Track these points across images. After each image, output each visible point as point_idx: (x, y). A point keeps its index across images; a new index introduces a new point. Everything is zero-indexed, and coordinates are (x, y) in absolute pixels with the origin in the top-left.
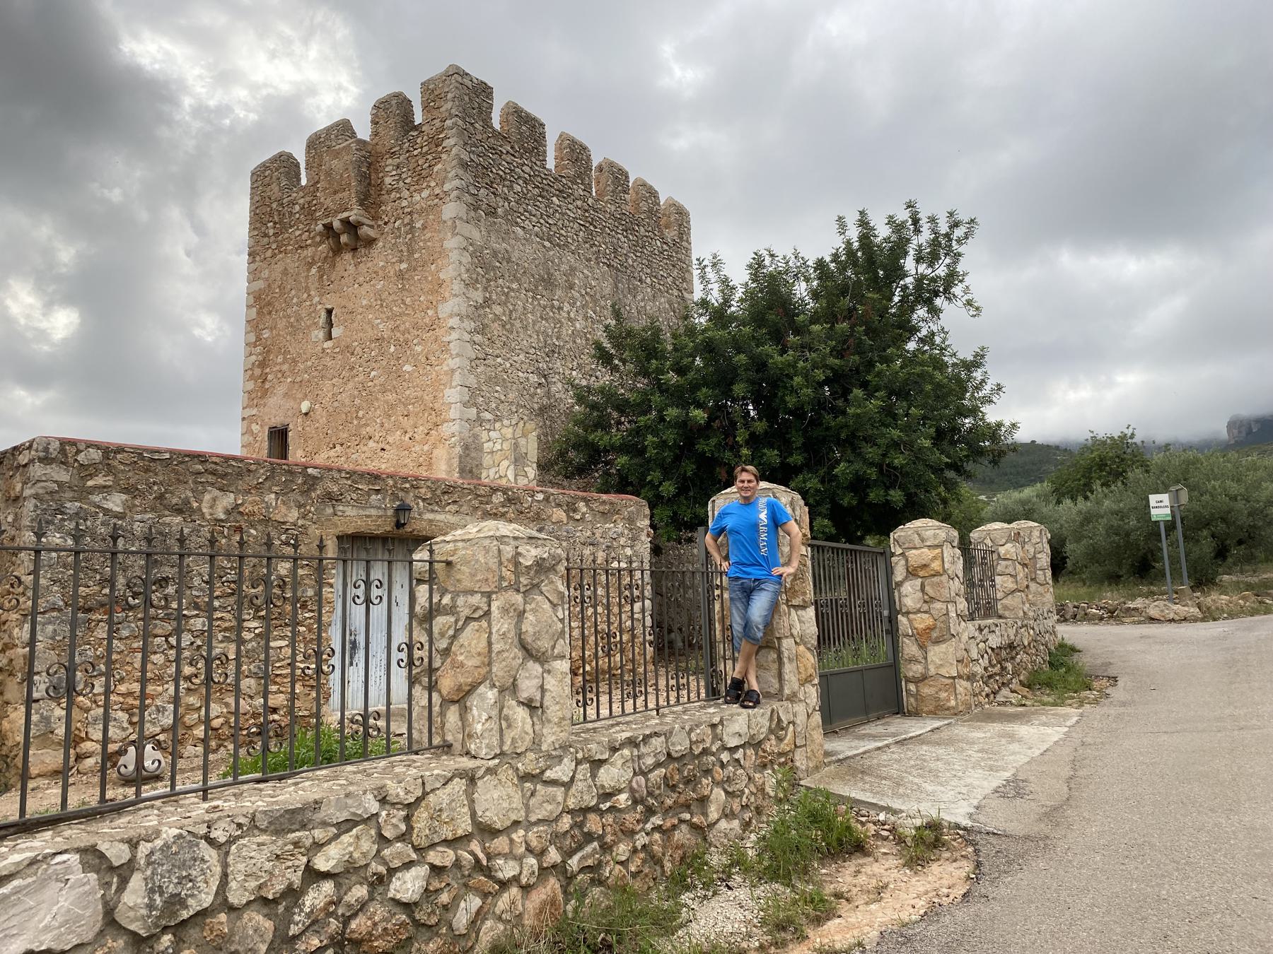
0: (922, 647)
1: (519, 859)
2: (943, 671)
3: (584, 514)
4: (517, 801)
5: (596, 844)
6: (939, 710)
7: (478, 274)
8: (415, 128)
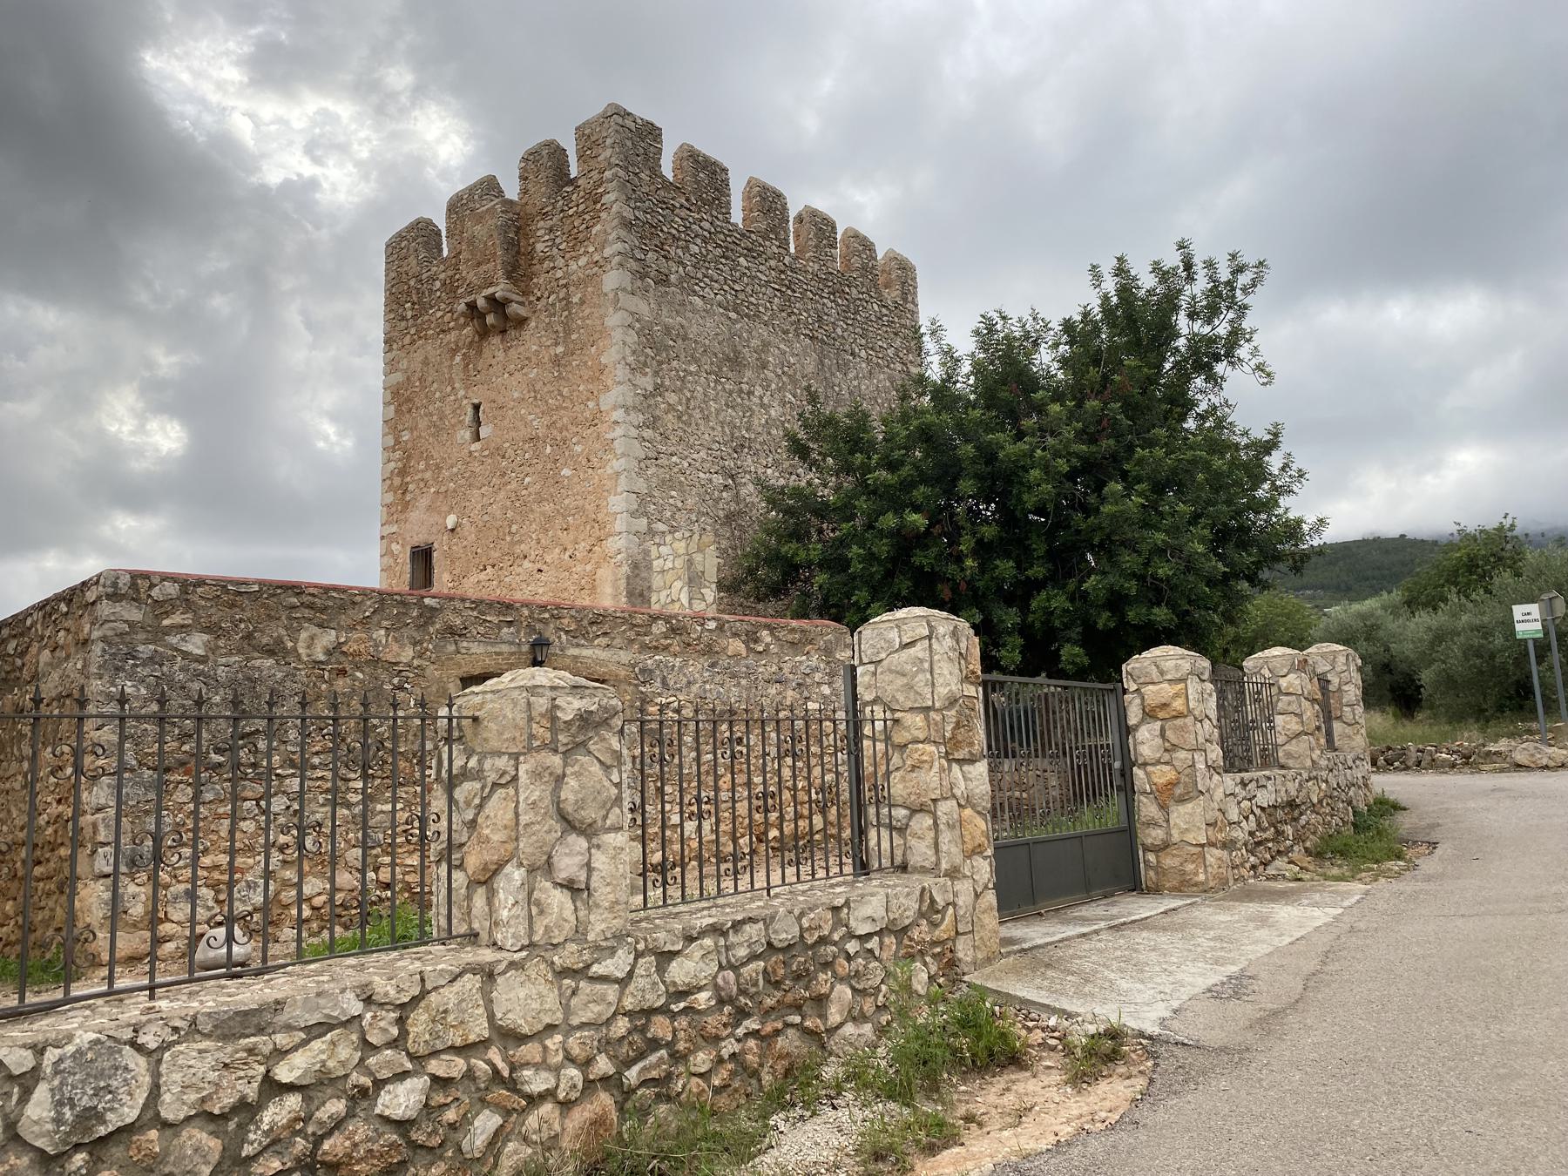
0: (1163, 807)
1: (556, 1070)
2: (1190, 838)
3: (768, 645)
4: (552, 1000)
5: (663, 1052)
6: (1184, 886)
7: (647, 356)
8: (572, 182)
